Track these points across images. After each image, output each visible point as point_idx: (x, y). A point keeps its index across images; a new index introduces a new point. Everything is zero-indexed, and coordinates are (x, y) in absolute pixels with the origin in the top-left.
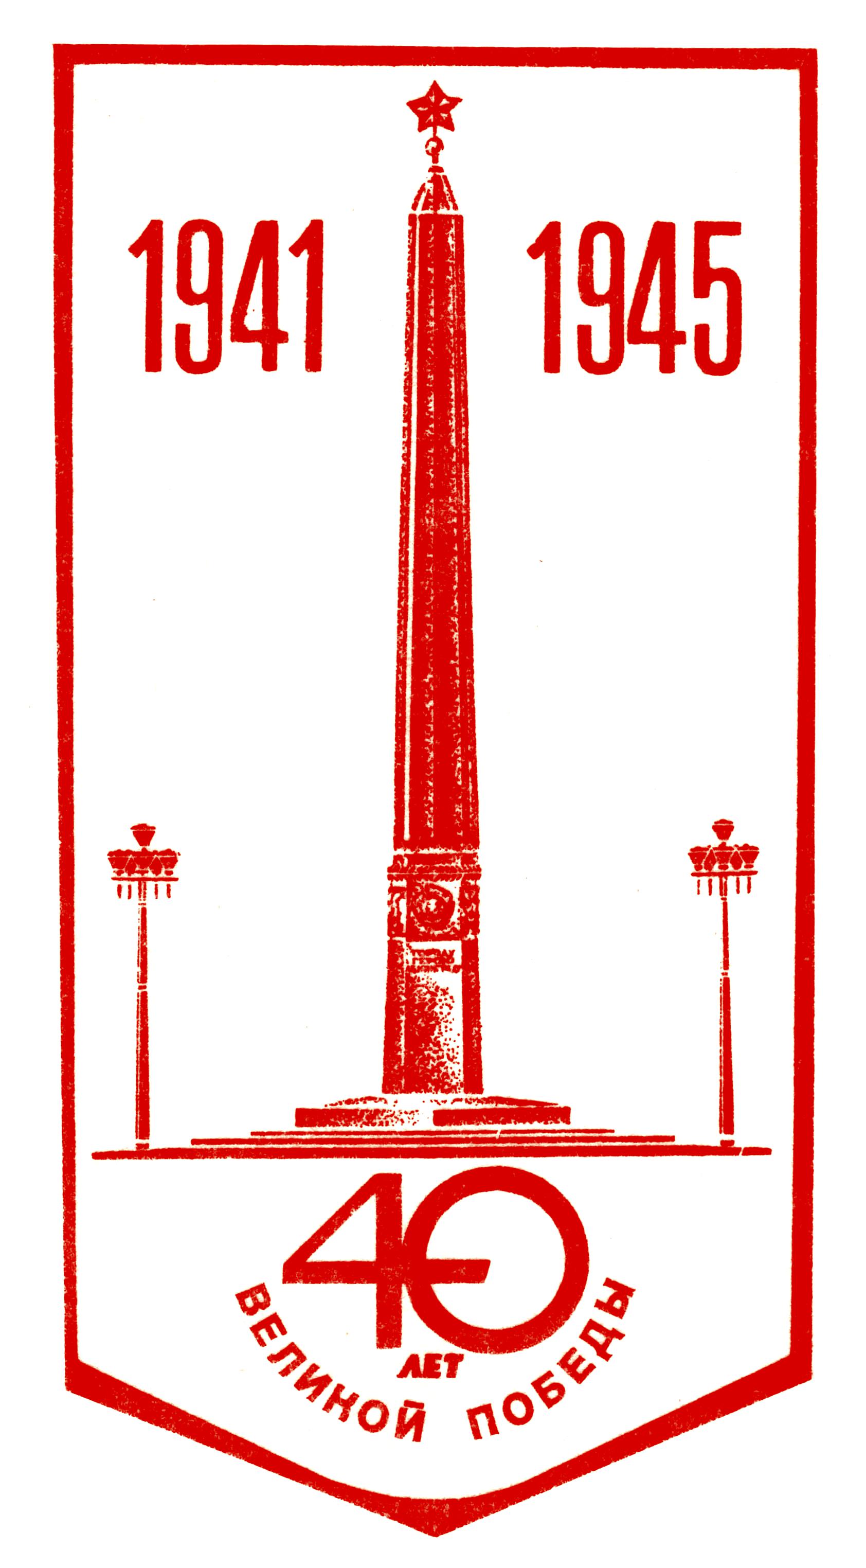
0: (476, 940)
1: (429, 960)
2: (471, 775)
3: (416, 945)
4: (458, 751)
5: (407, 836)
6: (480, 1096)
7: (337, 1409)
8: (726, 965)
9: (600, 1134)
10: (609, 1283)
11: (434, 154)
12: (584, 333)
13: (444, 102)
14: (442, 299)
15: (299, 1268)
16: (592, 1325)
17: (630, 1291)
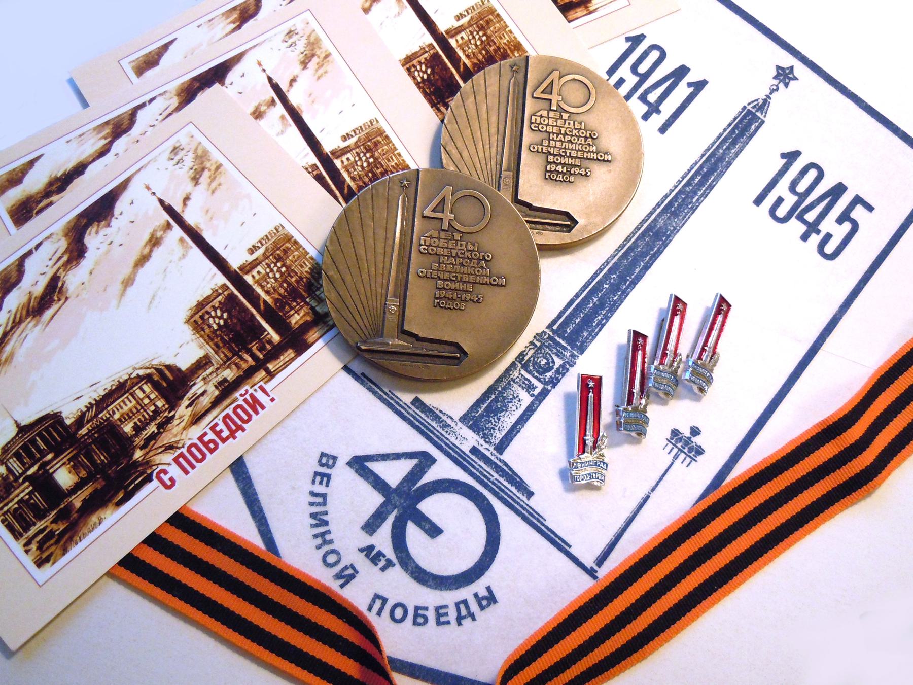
0: (550, 391)
1: (524, 383)
2: (601, 326)
3: (523, 372)
4: (604, 312)
5: (555, 327)
6: (499, 456)
7: (319, 541)
8: (653, 490)
9: (540, 518)
10: (489, 589)
11: (773, 91)
12: (780, 200)
13: (791, 76)
14: (734, 143)
15: (359, 464)
16: (465, 602)
17: (495, 601)
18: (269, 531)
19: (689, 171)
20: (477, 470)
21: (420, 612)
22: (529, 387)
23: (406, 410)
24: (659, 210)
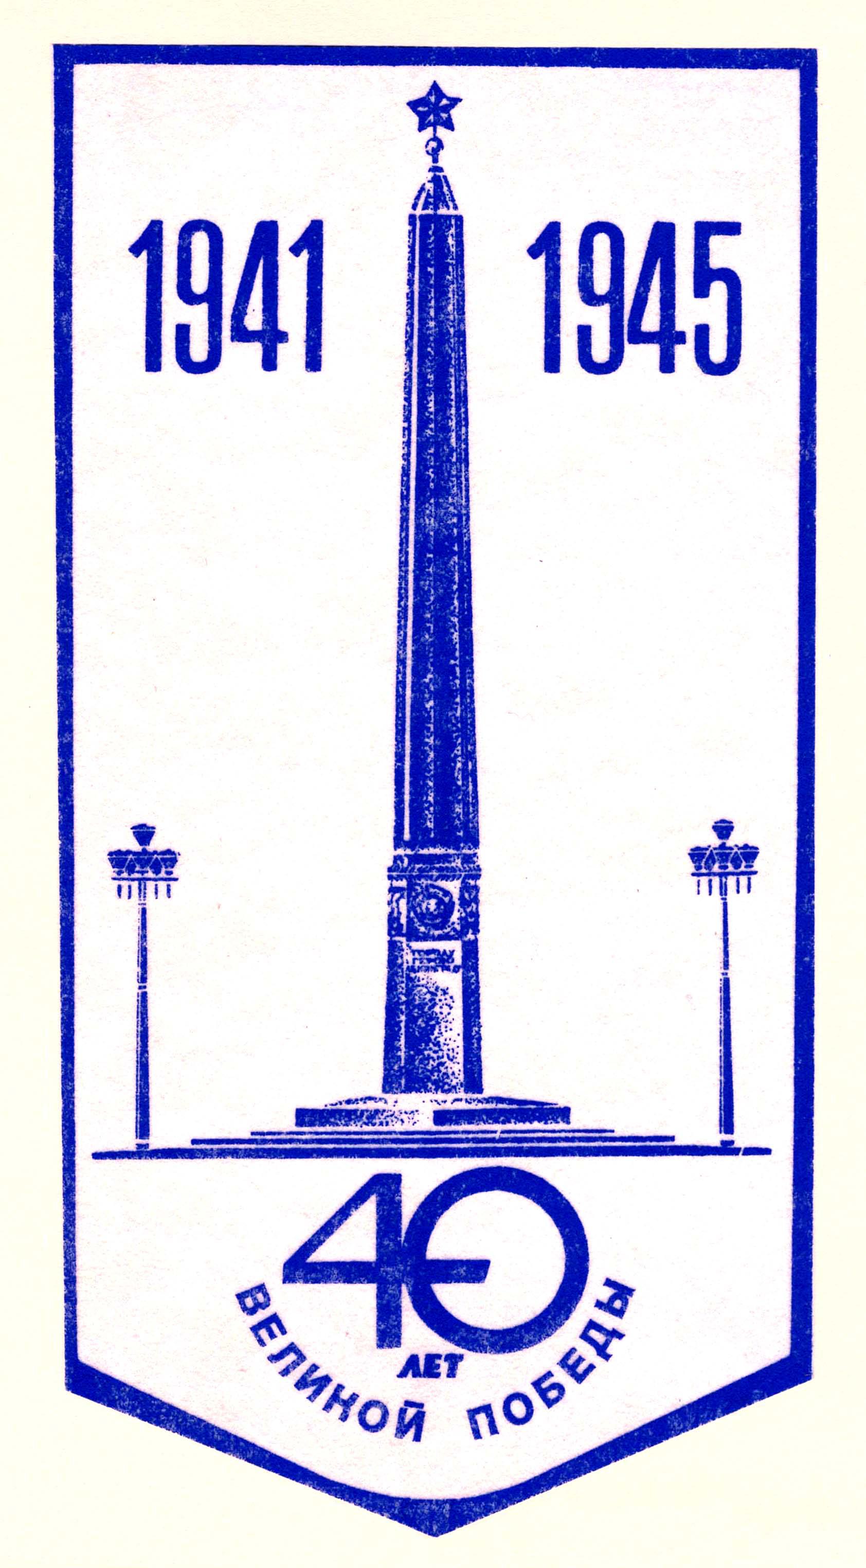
0: (476, 940)
1: (430, 961)
2: (471, 775)
3: (416, 945)
4: (458, 751)
5: (407, 836)
6: (480, 1096)
7: (337, 1409)
8: (726, 965)
9: (600, 1134)
10: (609, 1283)
11: (434, 154)
12: (584, 333)
13: (444, 102)
14: (441, 293)
15: (301, 1267)
17: (630, 1291)
18: (263, 1451)
19: (408, 399)
20: (468, 1140)
21: (545, 1385)
22: (443, 961)
23: (299, 1141)
24: (412, 506)
